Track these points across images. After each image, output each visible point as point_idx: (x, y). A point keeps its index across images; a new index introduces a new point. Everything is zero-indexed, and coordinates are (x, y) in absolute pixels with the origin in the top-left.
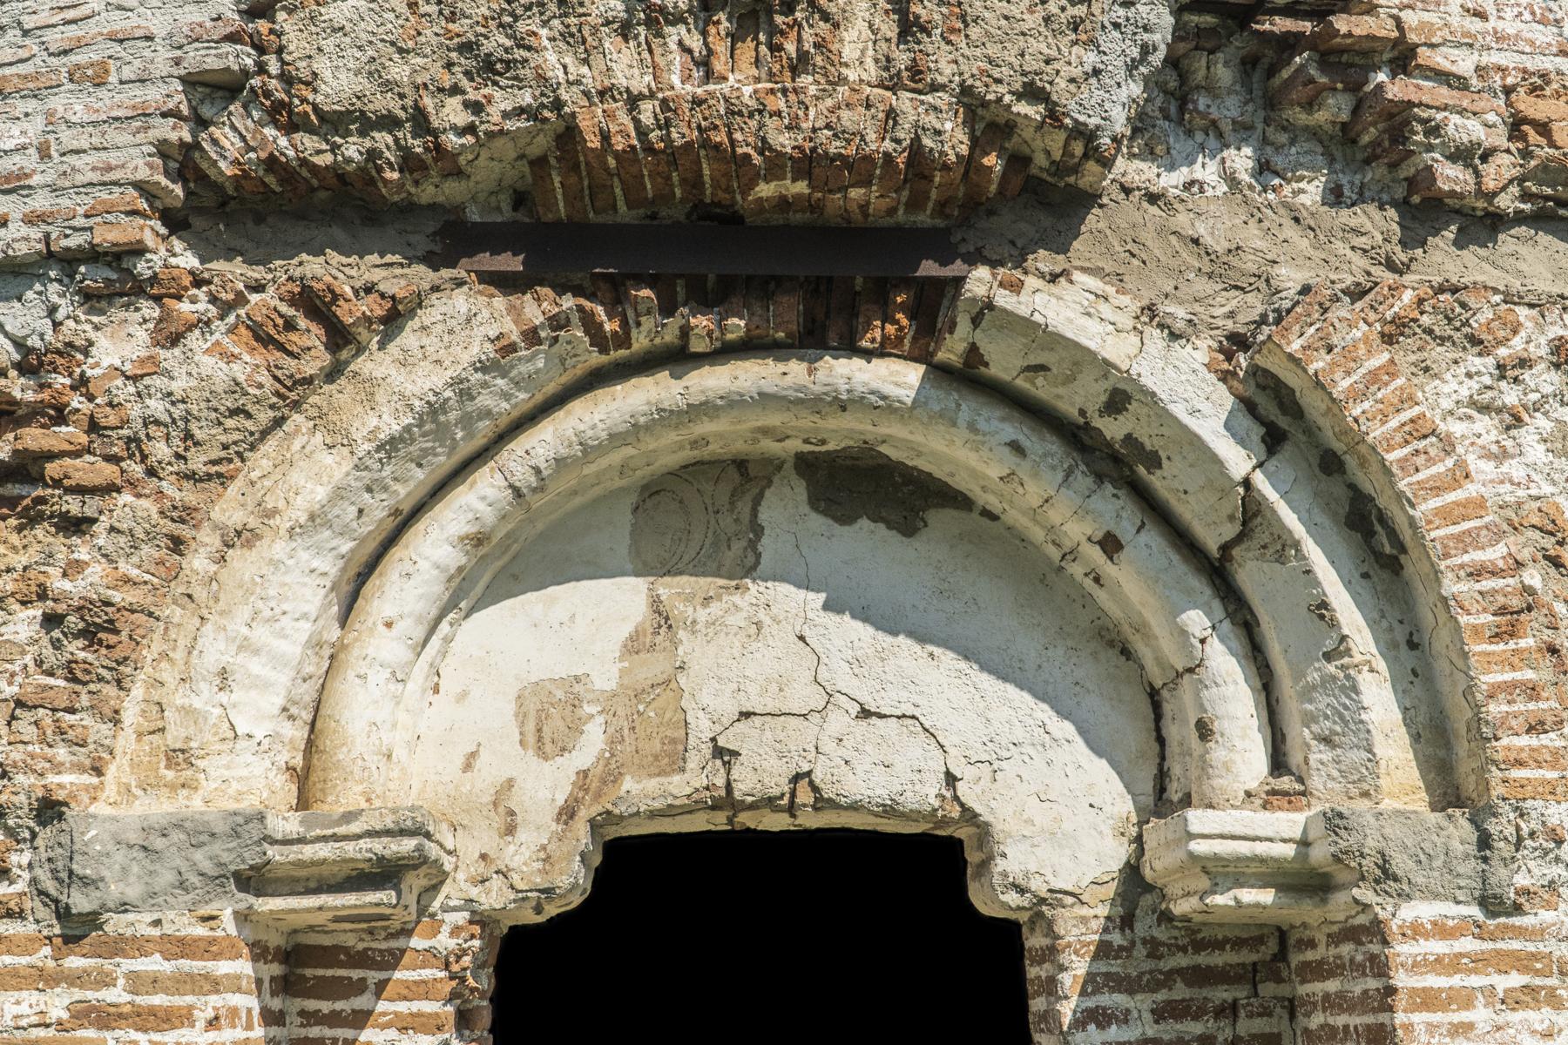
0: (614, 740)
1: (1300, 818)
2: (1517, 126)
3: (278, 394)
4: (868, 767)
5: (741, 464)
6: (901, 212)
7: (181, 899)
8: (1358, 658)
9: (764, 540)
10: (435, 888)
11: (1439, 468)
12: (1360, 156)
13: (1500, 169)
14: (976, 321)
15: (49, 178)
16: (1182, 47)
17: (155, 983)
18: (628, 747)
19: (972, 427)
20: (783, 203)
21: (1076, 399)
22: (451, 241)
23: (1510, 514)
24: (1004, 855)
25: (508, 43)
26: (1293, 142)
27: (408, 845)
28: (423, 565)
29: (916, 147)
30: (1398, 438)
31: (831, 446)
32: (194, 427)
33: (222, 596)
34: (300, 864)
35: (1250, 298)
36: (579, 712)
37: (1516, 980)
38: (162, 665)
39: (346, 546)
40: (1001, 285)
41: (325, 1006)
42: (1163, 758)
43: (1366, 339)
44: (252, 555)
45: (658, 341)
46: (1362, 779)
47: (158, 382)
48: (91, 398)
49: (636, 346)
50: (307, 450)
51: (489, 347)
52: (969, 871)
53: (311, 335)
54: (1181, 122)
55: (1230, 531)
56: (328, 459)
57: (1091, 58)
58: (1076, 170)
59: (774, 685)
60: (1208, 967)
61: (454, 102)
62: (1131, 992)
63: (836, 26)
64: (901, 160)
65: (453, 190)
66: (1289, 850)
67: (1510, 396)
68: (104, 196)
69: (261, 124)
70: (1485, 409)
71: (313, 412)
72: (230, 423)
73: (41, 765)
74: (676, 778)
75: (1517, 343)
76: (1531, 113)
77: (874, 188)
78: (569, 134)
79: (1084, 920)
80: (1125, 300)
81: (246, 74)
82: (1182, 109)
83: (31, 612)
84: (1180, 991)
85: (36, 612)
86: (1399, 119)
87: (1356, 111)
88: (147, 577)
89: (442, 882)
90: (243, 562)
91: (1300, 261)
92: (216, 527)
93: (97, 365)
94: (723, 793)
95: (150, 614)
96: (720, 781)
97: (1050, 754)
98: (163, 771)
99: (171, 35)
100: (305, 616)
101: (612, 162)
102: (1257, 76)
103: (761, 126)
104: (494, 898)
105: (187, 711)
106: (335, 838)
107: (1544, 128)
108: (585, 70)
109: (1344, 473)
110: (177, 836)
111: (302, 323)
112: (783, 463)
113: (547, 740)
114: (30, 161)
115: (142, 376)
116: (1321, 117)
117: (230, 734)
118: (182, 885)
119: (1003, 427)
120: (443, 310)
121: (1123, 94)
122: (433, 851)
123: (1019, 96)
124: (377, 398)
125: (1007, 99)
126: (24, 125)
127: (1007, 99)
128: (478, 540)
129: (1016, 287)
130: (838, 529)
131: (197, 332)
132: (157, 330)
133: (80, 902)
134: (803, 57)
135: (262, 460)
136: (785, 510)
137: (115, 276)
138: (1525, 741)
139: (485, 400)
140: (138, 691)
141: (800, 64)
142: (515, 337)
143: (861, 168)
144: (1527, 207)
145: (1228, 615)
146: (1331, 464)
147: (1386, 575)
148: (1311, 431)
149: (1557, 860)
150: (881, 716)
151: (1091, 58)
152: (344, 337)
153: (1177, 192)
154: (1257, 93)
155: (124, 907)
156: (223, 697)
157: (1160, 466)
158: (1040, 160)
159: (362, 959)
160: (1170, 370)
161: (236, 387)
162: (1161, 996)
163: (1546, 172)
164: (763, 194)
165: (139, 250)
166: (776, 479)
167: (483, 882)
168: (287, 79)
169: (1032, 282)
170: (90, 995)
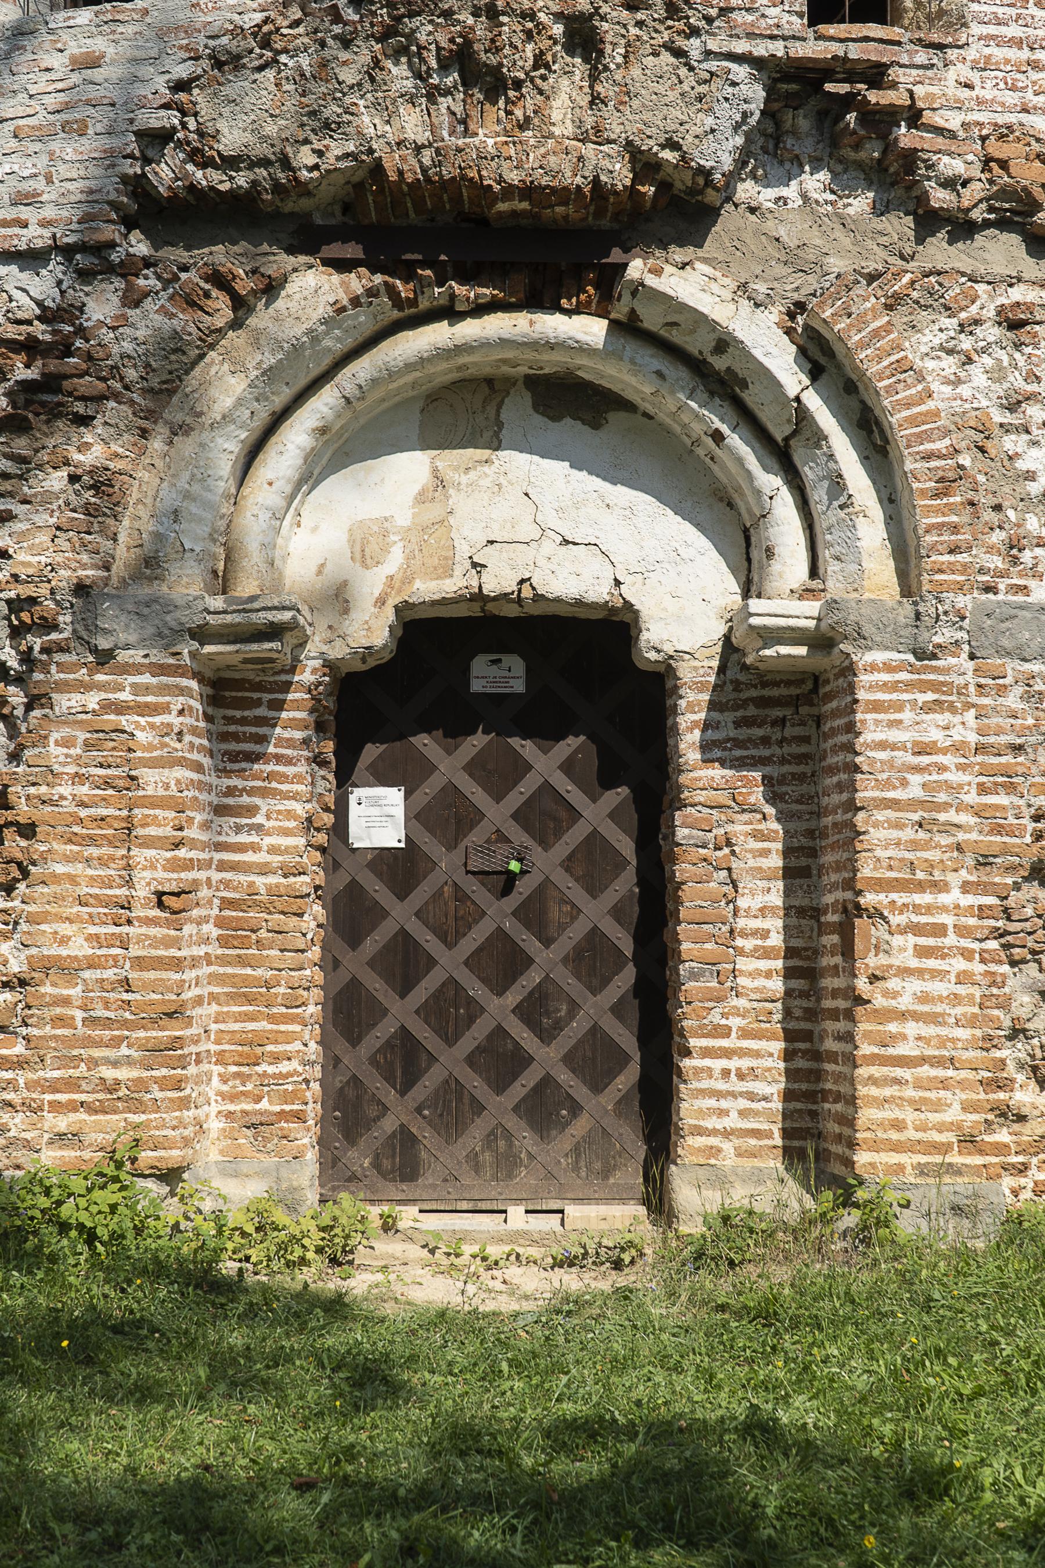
0: (409, 558)
1: (817, 605)
2: (987, 161)
5: (489, 381)
8: (857, 508)
10: (302, 645)
11: (913, 391)
13: (975, 191)
14: (634, 293)
15: (53, 196)
16: (776, 106)
17: (147, 689)
18: (417, 563)
19: (632, 361)
20: (514, 213)
21: (697, 344)
22: (307, 239)
23: (957, 419)
25: (340, 111)
26: (845, 171)
27: (287, 615)
28: (290, 447)
29: (596, 180)
30: (888, 373)
31: (546, 371)
37: (930, 696)
39: (244, 435)
40: (650, 271)
41: (238, 714)
42: (749, 571)
43: (873, 309)
44: (189, 440)
47: (127, 330)
48: (87, 341)
49: (421, 307)
51: (329, 309)
53: (221, 304)
54: (775, 155)
55: (788, 430)
56: (232, 380)
57: (710, 121)
58: (701, 192)
61: (306, 149)
62: (721, 711)
63: (548, 98)
64: (587, 190)
65: (305, 204)
66: (811, 624)
67: (966, 343)
69: (184, 162)
70: (950, 352)
71: (222, 350)
72: (173, 357)
73: (73, 565)
74: (448, 581)
75: (974, 309)
76: (997, 155)
78: (378, 167)
79: (695, 668)
80: (727, 281)
81: (174, 129)
82: (776, 146)
83: (59, 474)
84: (751, 711)
85: (63, 473)
86: (910, 158)
87: (884, 152)
92: (166, 422)
93: (88, 320)
96: (475, 583)
97: (680, 568)
99: (126, 103)
101: (405, 188)
102: (827, 124)
103: (499, 167)
106: (245, 611)
107: (1004, 164)
108: (387, 128)
111: (215, 293)
114: (40, 184)
116: (862, 155)
118: (160, 635)
119: (652, 360)
121: (730, 145)
122: (301, 621)
123: (663, 147)
125: (655, 149)
126: (34, 160)
127: (655, 149)
128: (323, 431)
129: (657, 272)
130: (551, 424)
132: (124, 297)
133: (103, 643)
134: (527, 119)
136: (517, 408)
138: (947, 558)
139: (327, 343)
140: (126, 522)
141: (524, 125)
142: (345, 302)
143: (563, 195)
144: (992, 216)
147: (879, 457)
148: (839, 367)
149: (961, 628)
151: (710, 121)
153: (770, 205)
154: (827, 135)
155: (127, 647)
156: (176, 527)
158: (678, 185)
159: (259, 687)
160: (753, 327)
161: (176, 335)
162: (740, 713)
163: (1004, 193)
165: (112, 245)
168: (201, 134)
169: (669, 269)
170: (110, 696)
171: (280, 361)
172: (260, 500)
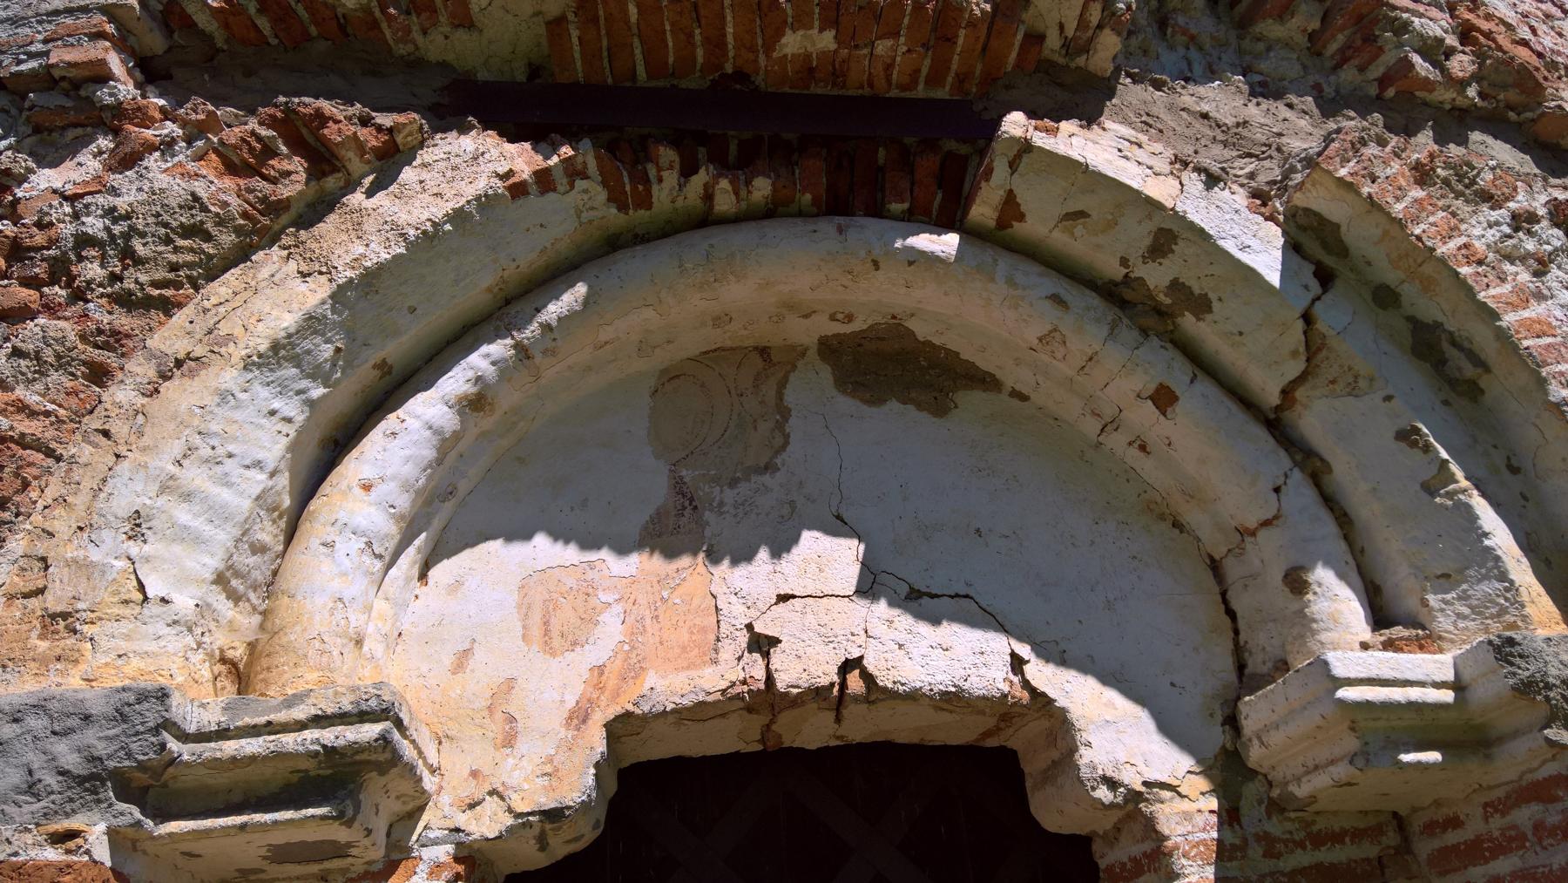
0: (635, 631)
3: (245, 215)
4: (925, 650)
6: (921, 86)
7: (26, 808)
9: (792, 421)
12: (1329, 64)
14: (1013, 165)
19: (1011, 282)
24: (1089, 745)
27: (369, 732)
31: (603, 820)
32: (138, 246)
33: (147, 430)
34: (215, 764)
35: (1267, 163)
36: (593, 601)
38: (56, 512)
42: (1236, 632)
44: (196, 384)
45: (680, 203)
46: (1503, 611)
50: (276, 279)
52: (1029, 784)
56: (300, 287)
59: (814, 566)
60: (1332, 865)
68: (69, 21)
74: (709, 671)
77: (902, 39)
79: (1187, 816)
80: (1158, 147)
88: (51, 407)
89: (421, 809)
90: (181, 394)
91: (1302, 135)
92: (152, 356)
94: (762, 686)
95: (50, 453)
96: (760, 673)
98: (34, 641)
100: (258, 465)
104: (487, 824)
105: (82, 566)
109: (1400, 306)
110: (36, 723)
112: (806, 349)
113: (555, 633)
115: (82, 196)
117: (139, 597)
120: (447, 149)
124: (365, 227)
131: (157, 154)
135: (219, 289)
137: (69, 104)
145: (1296, 464)
146: (1385, 297)
150: (933, 596)
152: (329, 162)
156: (134, 548)
157: (1209, 310)
164: (788, 51)
166: (800, 364)
167: (472, 806)
171: (396, 257)
172: (342, 516)
